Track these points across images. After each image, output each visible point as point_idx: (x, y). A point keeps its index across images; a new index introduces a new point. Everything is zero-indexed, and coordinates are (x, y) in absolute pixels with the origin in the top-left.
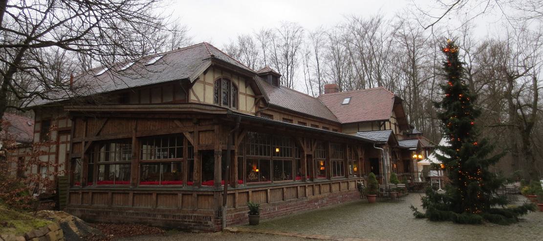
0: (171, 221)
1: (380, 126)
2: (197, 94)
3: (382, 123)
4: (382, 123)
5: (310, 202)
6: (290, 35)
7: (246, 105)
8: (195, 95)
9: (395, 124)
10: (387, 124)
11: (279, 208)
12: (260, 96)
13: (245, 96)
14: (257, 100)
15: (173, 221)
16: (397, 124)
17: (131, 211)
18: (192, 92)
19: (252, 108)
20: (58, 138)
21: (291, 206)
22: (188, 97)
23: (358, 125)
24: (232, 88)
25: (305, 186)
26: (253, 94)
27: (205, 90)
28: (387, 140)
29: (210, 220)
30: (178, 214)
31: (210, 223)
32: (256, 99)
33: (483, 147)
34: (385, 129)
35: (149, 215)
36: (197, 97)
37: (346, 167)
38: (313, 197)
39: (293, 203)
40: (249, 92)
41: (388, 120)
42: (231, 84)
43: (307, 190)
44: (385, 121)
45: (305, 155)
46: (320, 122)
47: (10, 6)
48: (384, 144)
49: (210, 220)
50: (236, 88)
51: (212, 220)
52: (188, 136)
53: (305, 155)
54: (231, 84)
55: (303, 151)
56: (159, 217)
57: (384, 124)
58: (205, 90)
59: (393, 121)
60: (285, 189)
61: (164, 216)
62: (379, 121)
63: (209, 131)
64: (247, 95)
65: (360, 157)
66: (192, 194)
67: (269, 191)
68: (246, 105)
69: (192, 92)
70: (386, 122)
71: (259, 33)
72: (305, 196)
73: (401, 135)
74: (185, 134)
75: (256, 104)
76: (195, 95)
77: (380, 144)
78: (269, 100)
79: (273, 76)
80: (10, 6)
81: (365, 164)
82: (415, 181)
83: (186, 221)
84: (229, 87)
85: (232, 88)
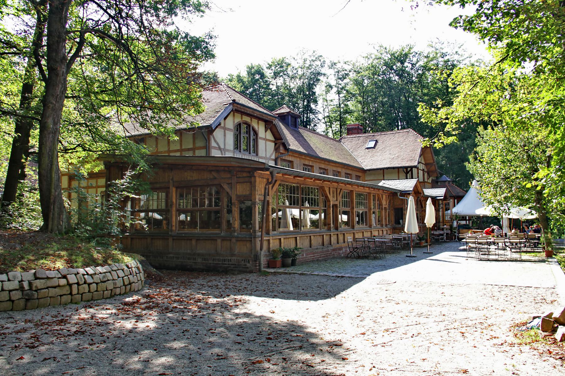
0: (211, 263)
1: (407, 173)
2: (218, 141)
3: (409, 169)
4: (409, 169)
5: (334, 250)
6: (308, 63)
7: (266, 151)
8: (215, 141)
9: (423, 170)
10: (415, 170)
11: (307, 255)
12: (280, 141)
13: (264, 141)
14: (277, 146)
15: (213, 263)
16: (426, 170)
17: (171, 255)
18: (212, 139)
19: (272, 154)
20: (70, 184)
21: (317, 253)
22: (209, 143)
23: (384, 173)
24: (252, 133)
25: (330, 235)
26: (273, 139)
27: (225, 136)
28: (412, 189)
29: (249, 263)
30: (218, 258)
31: (248, 265)
32: (276, 144)
33: (184, 345)
34: (412, 178)
35: (189, 259)
36: (218, 144)
37: (370, 217)
38: (338, 246)
39: (319, 250)
40: (269, 136)
41: (415, 167)
42: (251, 129)
43: (332, 238)
44: (412, 167)
45: (331, 205)
46: (342, 168)
47: (266, 155)
48: (409, 194)
49: (249, 263)
50: (256, 133)
51: (251, 262)
52: (226, 187)
53: (331, 205)
54: (251, 129)
55: (330, 201)
56: (199, 260)
57: (411, 170)
58: (225, 136)
59: (421, 167)
60: (312, 237)
61: (205, 259)
62: (406, 168)
63: (246, 182)
64: (266, 140)
65: (384, 206)
66: (231, 240)
67: (298, 238)
68: (266, 151)
69: (212, 139)
70: (414, 169)
71: (270, 63)
72: (331, 244)
73: (429, 183)
74: (222, 185)
75: (276, 149)
76: (215, 141)
77: (405, 194)
78: (289, 145)
79: (292, 117)
80: (266, 155)
81: (389, 214)
82: (99, 41)
83: (226, 264)
84: (248, 132)
85: (252, 133)
